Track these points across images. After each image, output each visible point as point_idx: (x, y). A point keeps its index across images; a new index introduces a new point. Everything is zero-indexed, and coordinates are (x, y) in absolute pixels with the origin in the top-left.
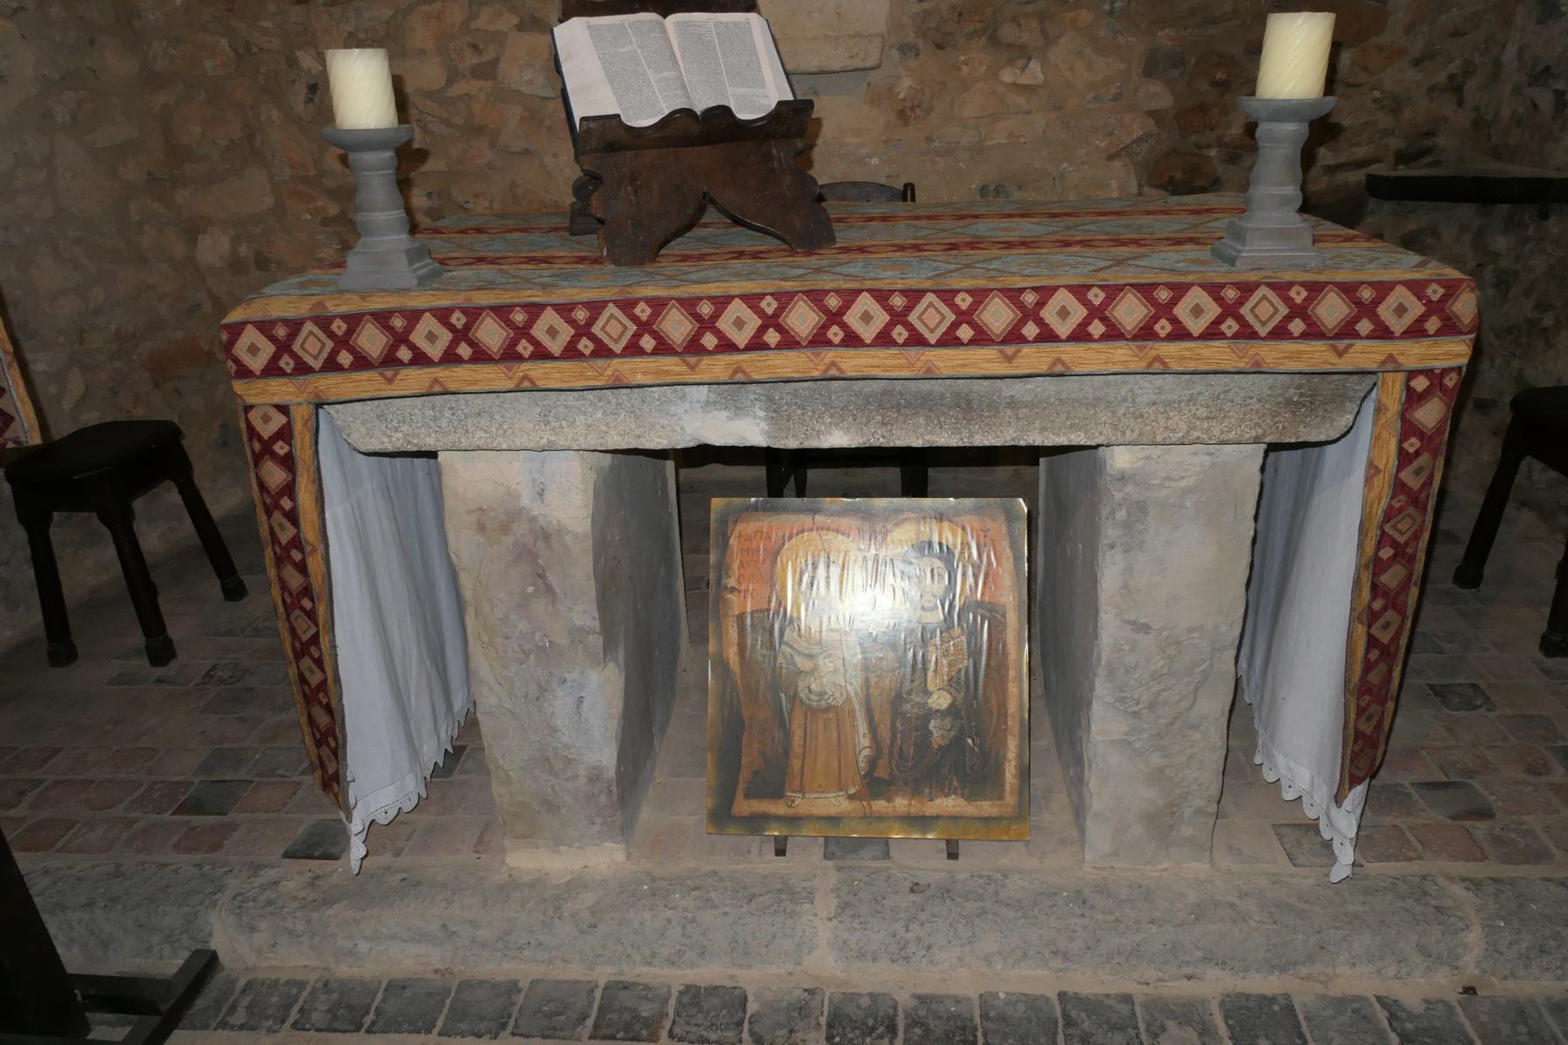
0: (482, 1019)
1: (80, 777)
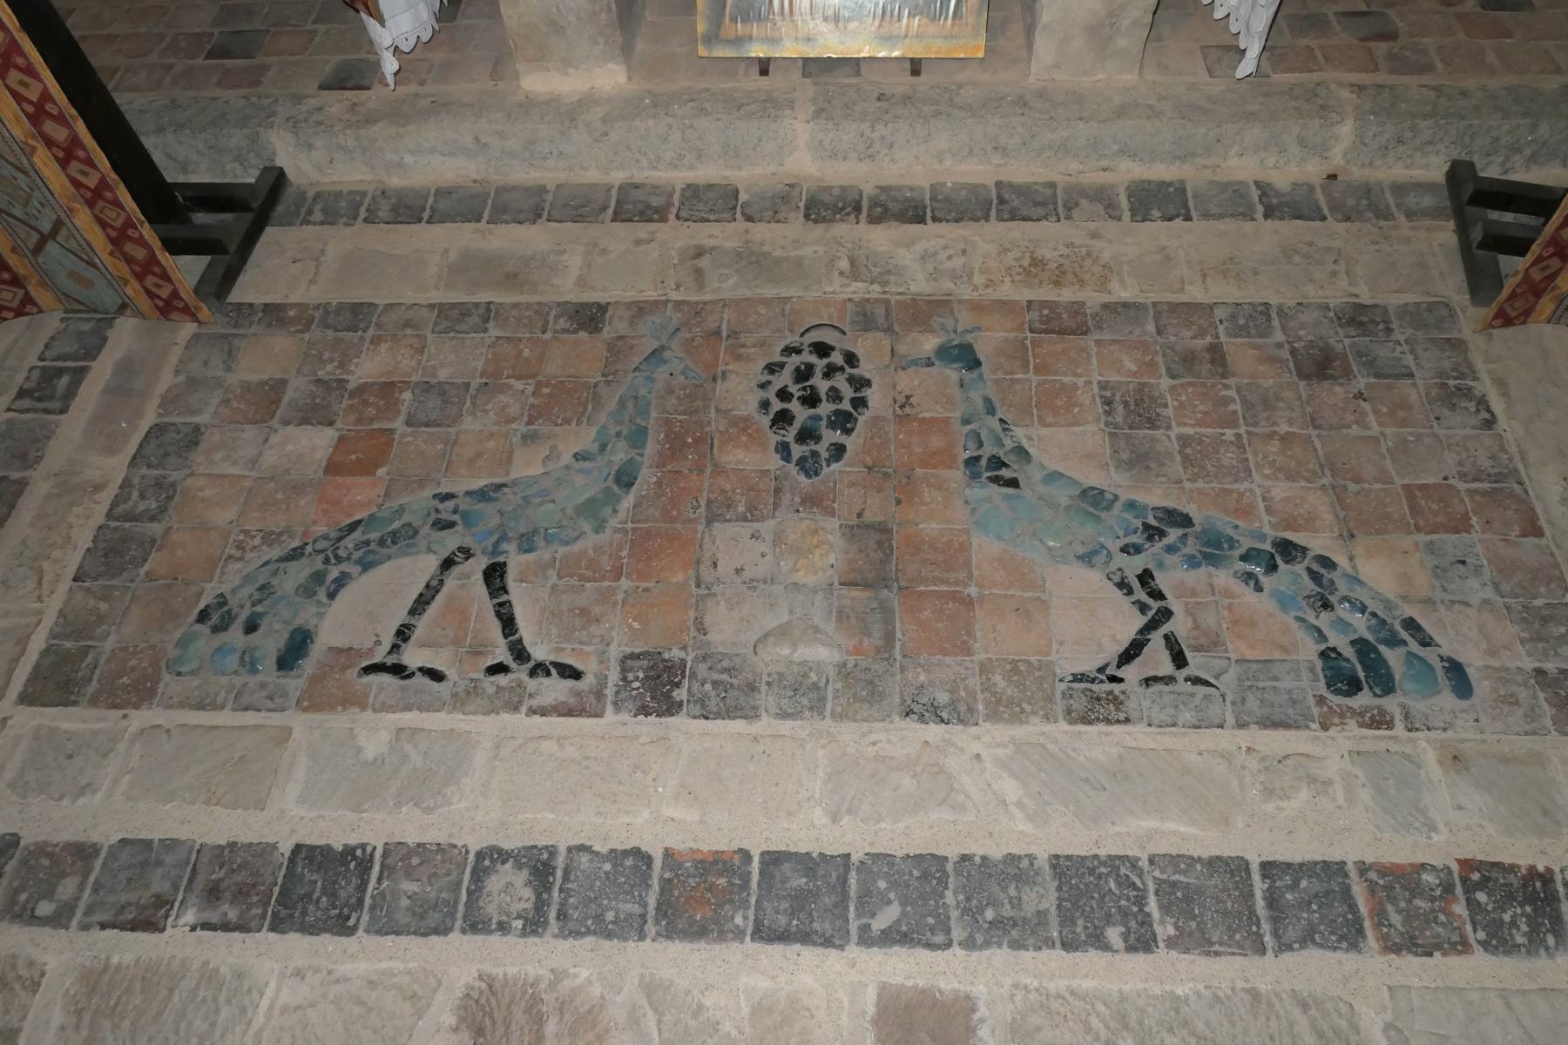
0: (520, 212)
1: (104, 32)
